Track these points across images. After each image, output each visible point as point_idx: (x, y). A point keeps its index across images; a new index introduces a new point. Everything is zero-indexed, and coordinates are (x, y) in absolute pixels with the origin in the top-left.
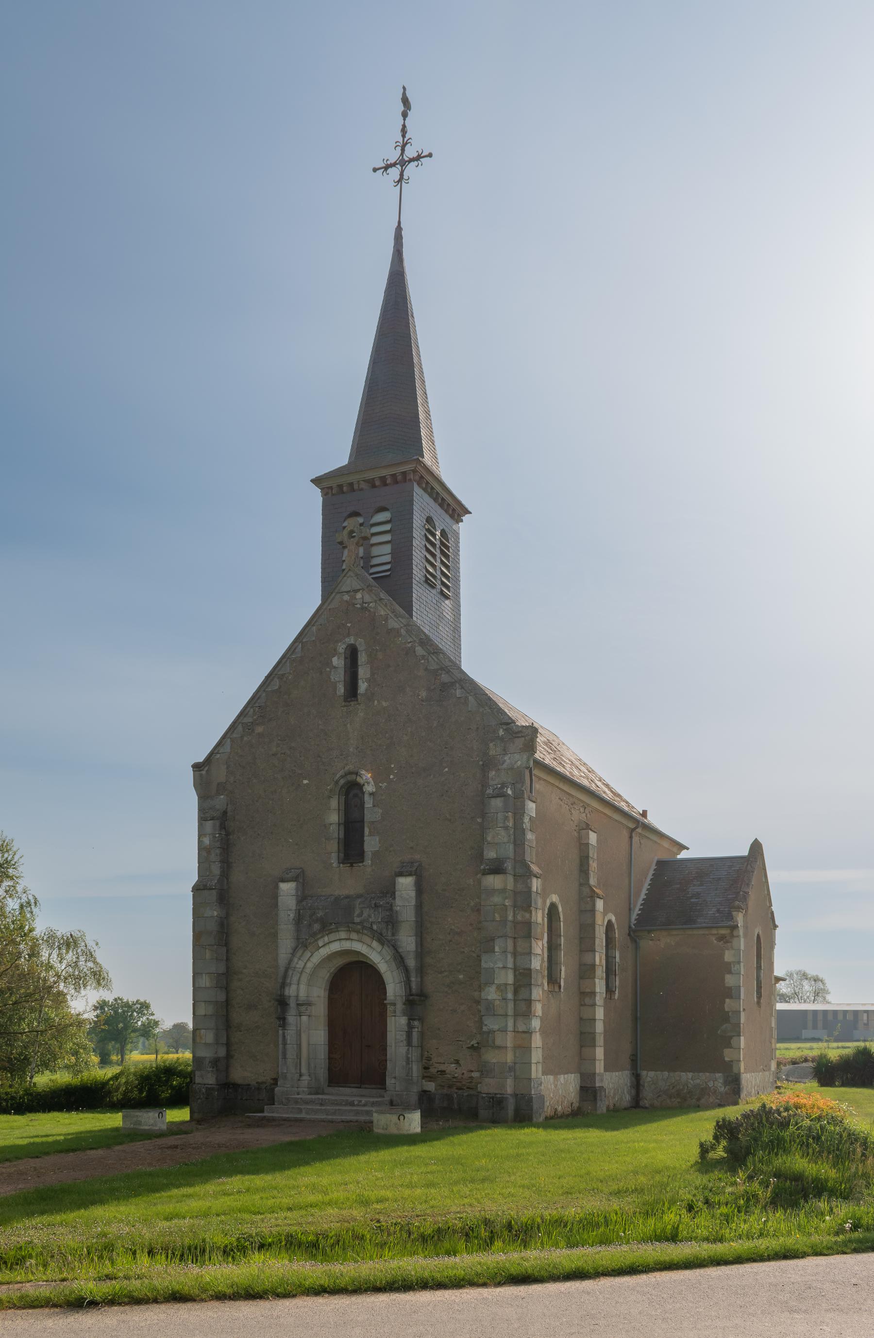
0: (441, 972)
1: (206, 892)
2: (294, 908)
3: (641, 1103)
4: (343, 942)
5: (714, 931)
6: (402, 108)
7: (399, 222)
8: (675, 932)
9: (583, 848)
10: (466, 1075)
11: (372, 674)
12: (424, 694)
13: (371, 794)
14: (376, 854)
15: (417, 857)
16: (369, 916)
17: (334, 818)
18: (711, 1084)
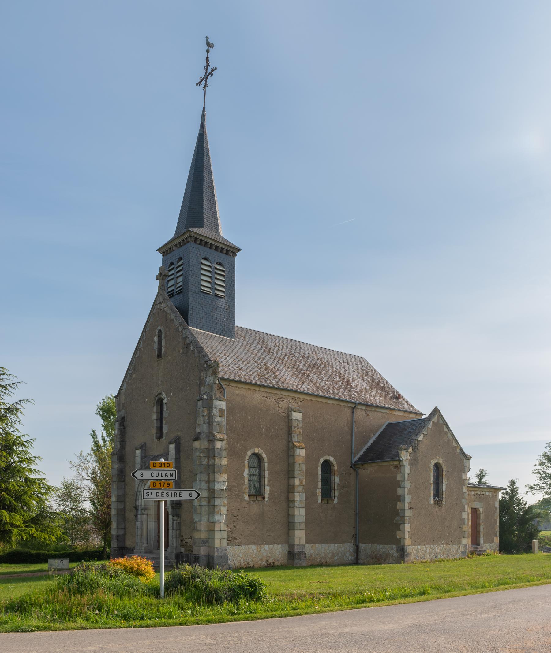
3: (359, 561)
5: (391, 463)
7: (204, 108)
8: (374, 465)
9: (289, 420)
18: (390, 551)
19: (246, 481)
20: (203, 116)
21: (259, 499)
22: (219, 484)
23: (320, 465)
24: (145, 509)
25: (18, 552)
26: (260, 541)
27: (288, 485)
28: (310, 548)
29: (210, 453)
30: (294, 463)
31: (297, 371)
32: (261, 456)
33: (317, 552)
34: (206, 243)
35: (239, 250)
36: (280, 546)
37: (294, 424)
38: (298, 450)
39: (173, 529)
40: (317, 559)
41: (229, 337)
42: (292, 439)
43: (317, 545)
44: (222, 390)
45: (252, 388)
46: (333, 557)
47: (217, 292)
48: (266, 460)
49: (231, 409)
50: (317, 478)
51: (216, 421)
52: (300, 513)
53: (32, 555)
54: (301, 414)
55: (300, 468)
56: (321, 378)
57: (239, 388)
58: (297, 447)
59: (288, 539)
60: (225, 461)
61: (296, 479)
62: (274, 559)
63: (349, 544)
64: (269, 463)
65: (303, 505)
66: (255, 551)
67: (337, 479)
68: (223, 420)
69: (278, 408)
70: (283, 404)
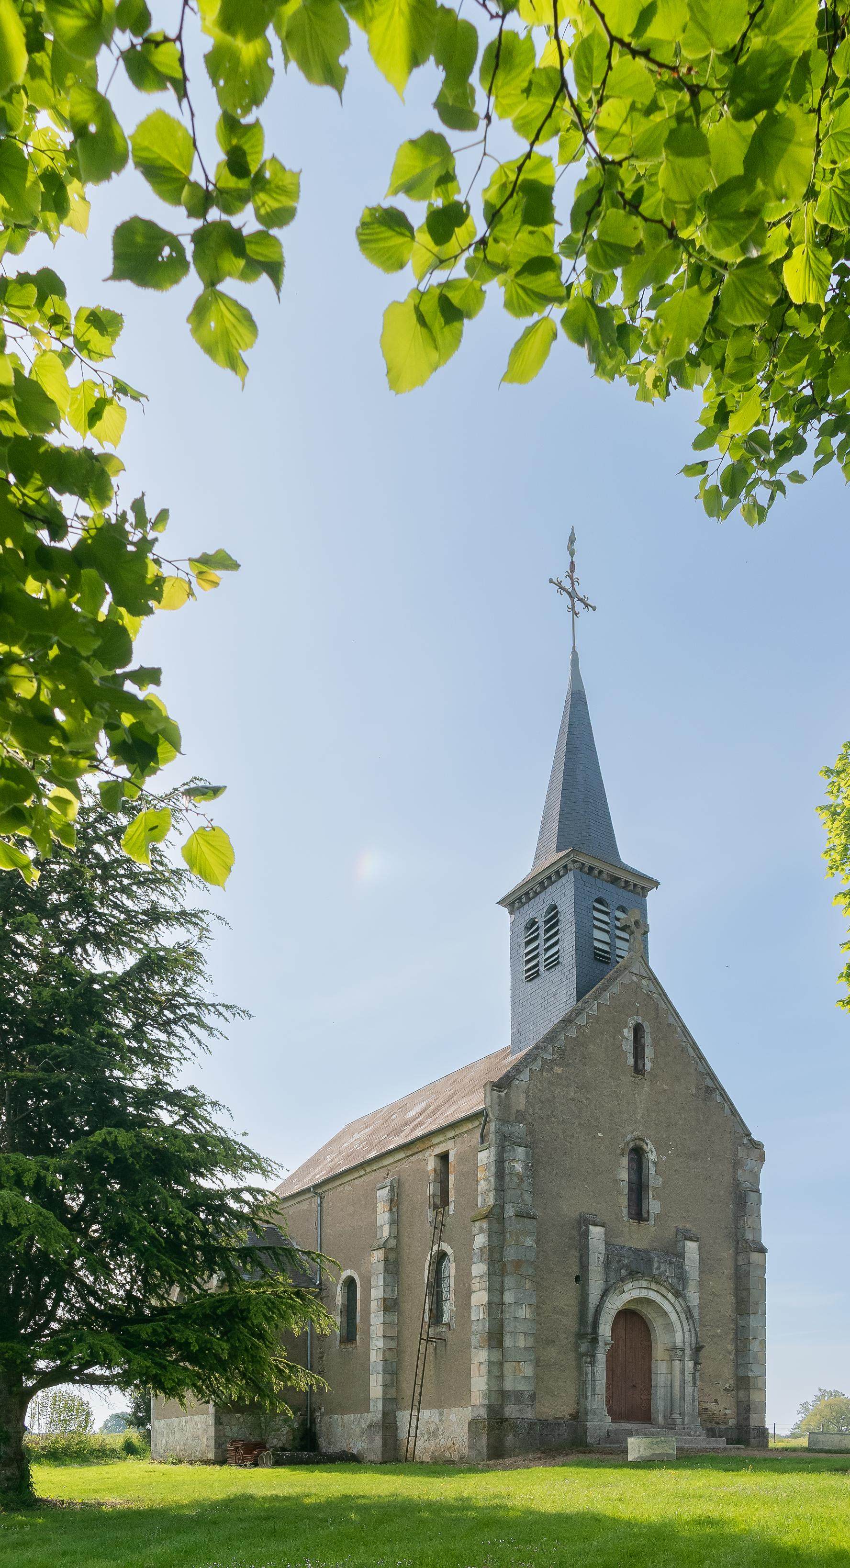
0: (705, 1326)
1: (527, 1221)
2: (603, 1251)
4: (642, 1290)
6: (575, 546)
7: (574, 647)
10: (722, 1412)
11: (656, 1057)
12: (693, 1090)
13: (655, 1163)
14: (657, 1216)
15: (689, 1226)
16: (665, 1270)
17: (624, 1175)
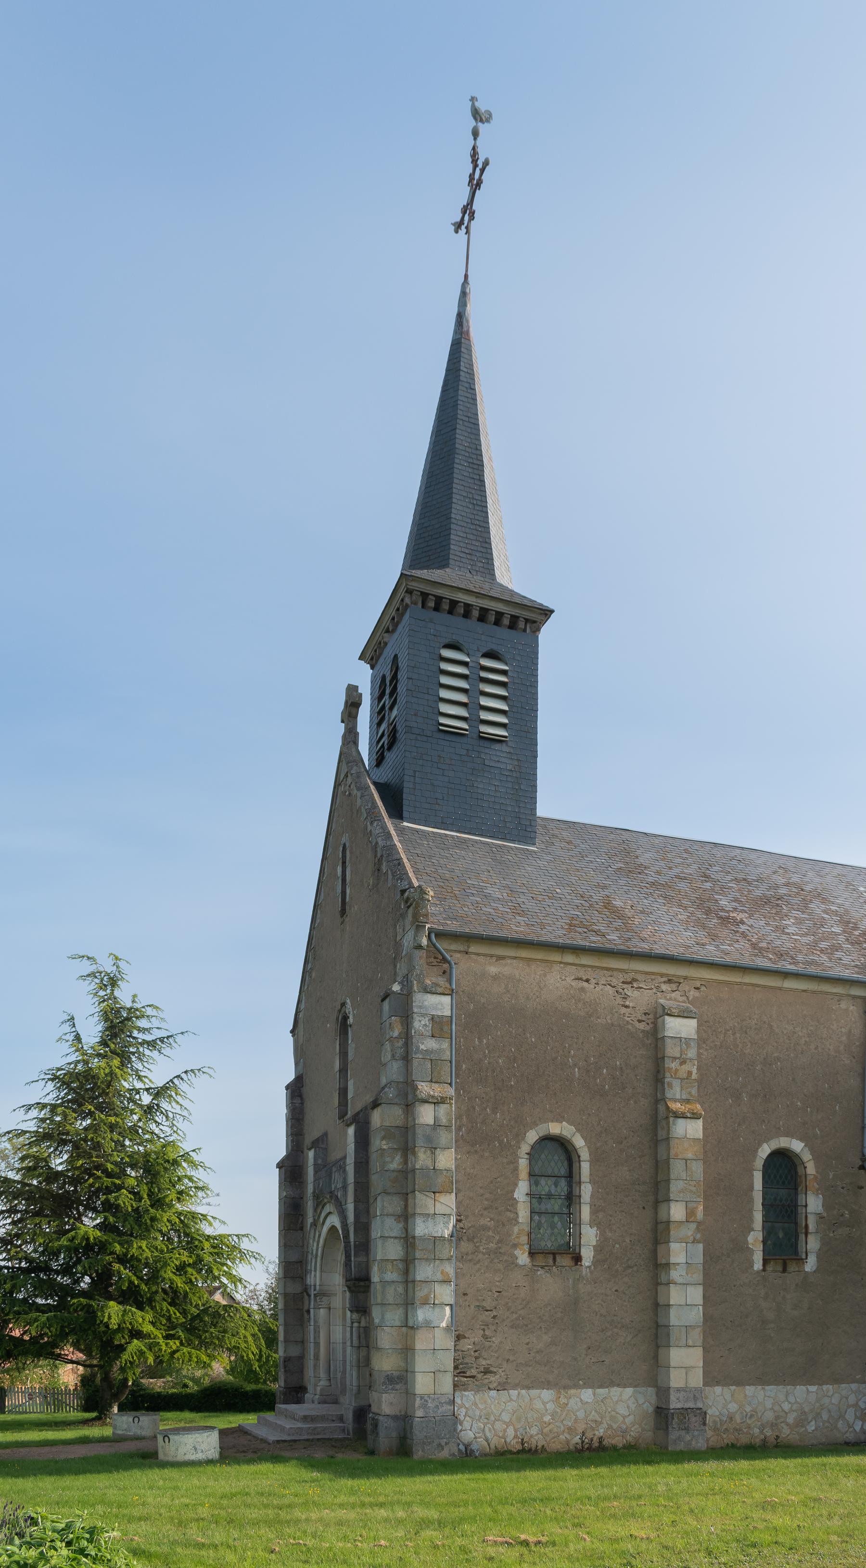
7: (466, 276)
9: (655, 1039)
19: (523, 1213)
20: (464, 294)
21: (565, 1261)
22: (430, 1223)
23: (759, 1163)
24: (322, 1294)
25: (219, 1388)
26: (569, 1379)
27: (656, 1223)
28: (728, 1397)
29: (406, 1138)
30: (668, 1159)
31: (708, 912)
32: (569, 1142)
33: (748, 1409)
34: (454, 603)
35: (547, 613)
36: (629, 1391)
37: (671, 1050)
38: (681, 1122)
39: (352, 1346)
40: (749, 1427)
41: (519, 842)
42: (663, 1092)
43: (750, 1390)
44: (446, 966)
45: (539, 955)
46: (801, 1421)
47: (484, 728)
48: (585, 1155)
49: (473, 1018)
50: (751, 1200)
51: (422, 1052)
52: (686, 1301)
53: (245, 1394)
54: (693, 1023)
55: (687, 1176)
56: (781, 929)
57: (500, 958)
58: (678, 1115)
59: (653, 1371)
60: (446, 1160)
61: (673, 1205)
62: (610, 1427)
63: (854, 1386)
64: (594, 1161)
65: (698, 1277)
66: (550, 1406)
67: (814, 1204)
68: (445, 1045)
69: (623, 1010)
70: (640, 998)
